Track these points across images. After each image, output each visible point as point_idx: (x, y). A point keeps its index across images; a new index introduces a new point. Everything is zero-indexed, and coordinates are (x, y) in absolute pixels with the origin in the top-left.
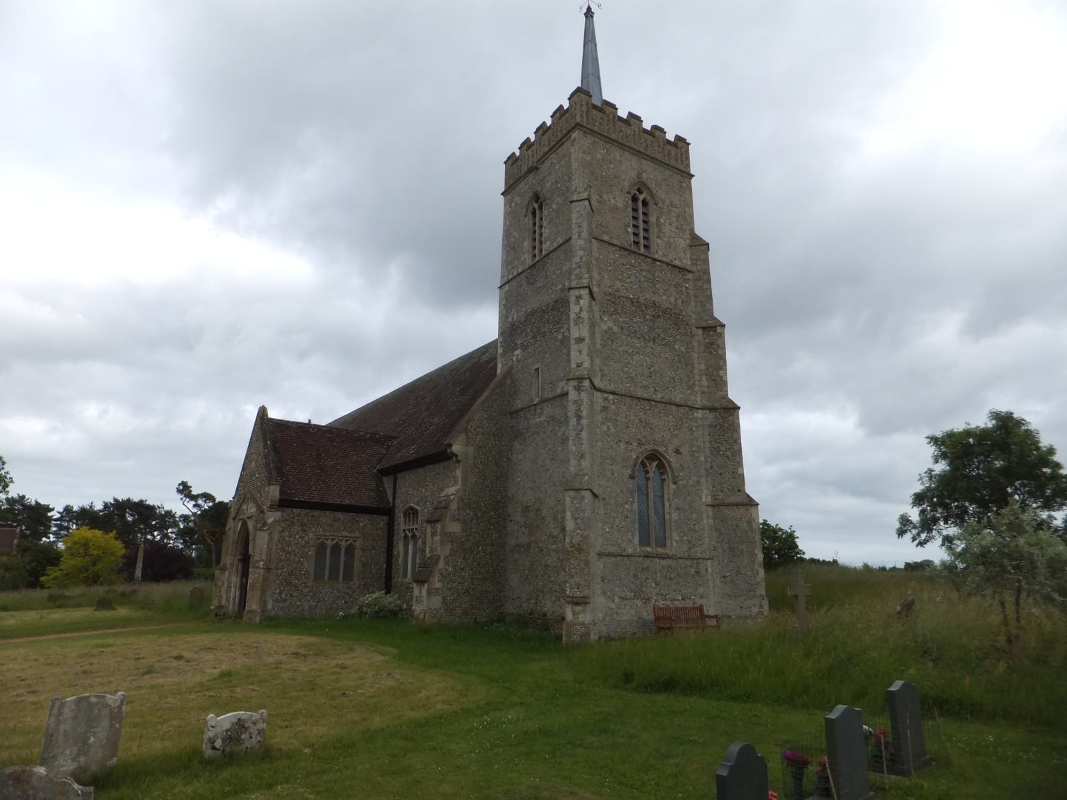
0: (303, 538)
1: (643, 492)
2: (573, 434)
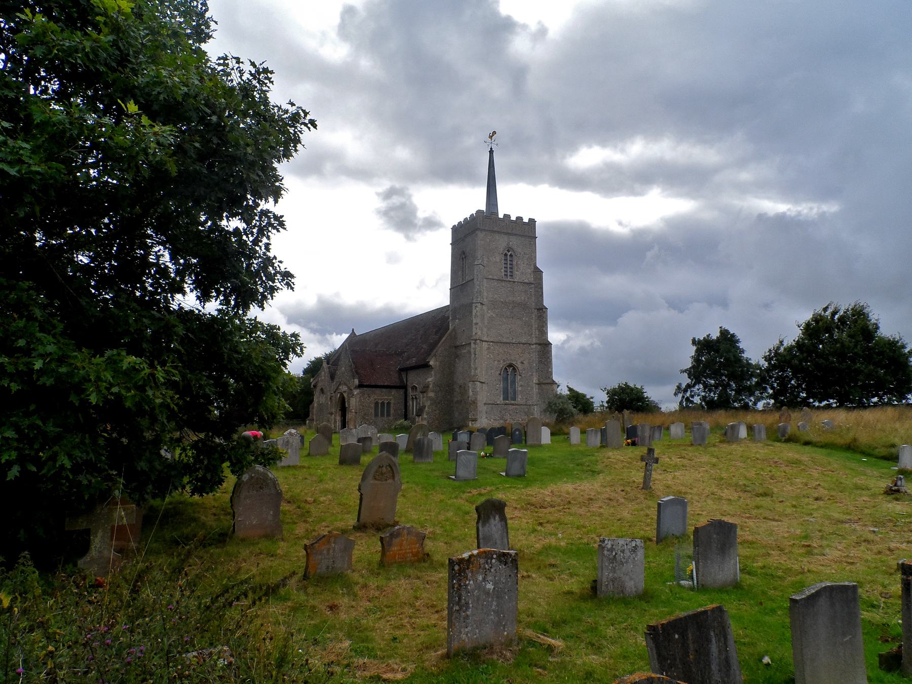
1: (506, 379)
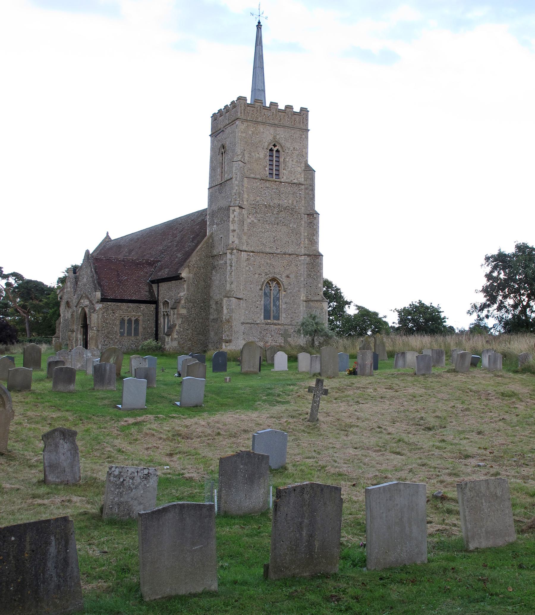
0: (113, 316)
2: (229, 273)
